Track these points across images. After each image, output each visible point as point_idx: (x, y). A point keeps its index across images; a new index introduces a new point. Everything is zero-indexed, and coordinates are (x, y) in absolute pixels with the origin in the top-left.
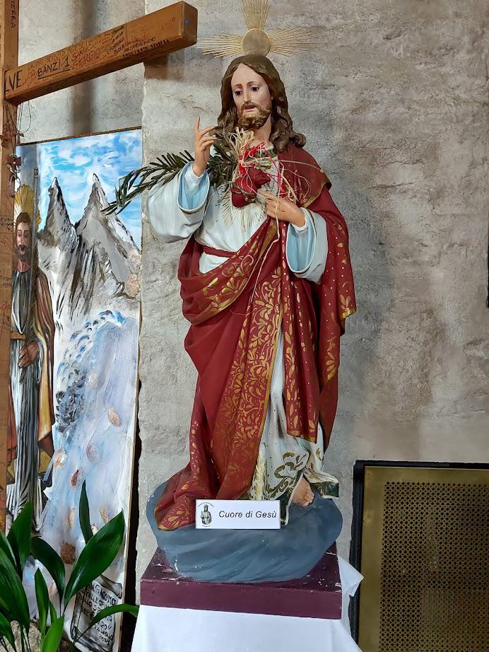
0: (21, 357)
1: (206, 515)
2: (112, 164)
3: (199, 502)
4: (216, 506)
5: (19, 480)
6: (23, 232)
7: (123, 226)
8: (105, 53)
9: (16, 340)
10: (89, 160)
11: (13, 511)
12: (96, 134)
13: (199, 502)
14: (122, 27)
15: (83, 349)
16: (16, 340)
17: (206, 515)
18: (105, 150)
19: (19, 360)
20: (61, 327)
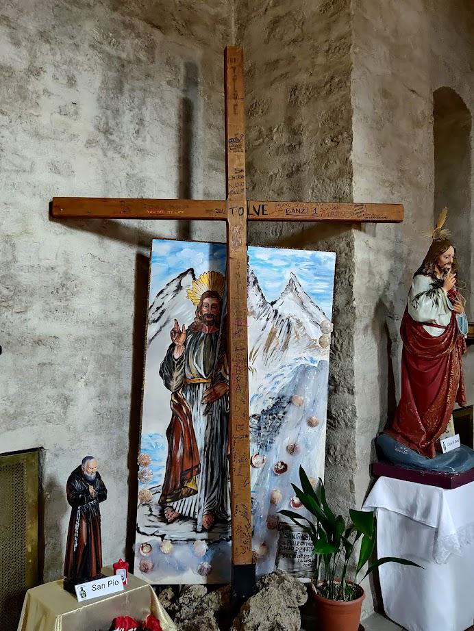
0: (205, 395)
1: (82, 592)
2: (309, 269)
3: (76, 587)
4: (88, 586)
5: (204, 490)
6: (210, 305)
7: (317, 307)
8: (350, 215)
9: (199, 384)
10: (286, 263)
11: (196, 516)
12: (193, 241)
13: (76, 587)
14: (362, 205)
15: (277, 383)
16: (199, 384)
17: (82, 592)
18: (302, 260)
19: (203, 399)
20: (254, 370)
